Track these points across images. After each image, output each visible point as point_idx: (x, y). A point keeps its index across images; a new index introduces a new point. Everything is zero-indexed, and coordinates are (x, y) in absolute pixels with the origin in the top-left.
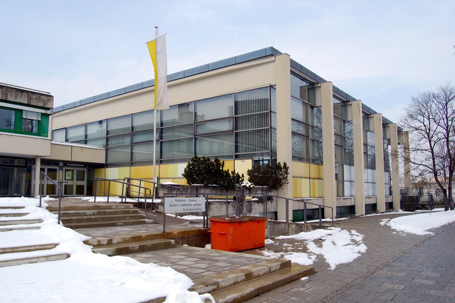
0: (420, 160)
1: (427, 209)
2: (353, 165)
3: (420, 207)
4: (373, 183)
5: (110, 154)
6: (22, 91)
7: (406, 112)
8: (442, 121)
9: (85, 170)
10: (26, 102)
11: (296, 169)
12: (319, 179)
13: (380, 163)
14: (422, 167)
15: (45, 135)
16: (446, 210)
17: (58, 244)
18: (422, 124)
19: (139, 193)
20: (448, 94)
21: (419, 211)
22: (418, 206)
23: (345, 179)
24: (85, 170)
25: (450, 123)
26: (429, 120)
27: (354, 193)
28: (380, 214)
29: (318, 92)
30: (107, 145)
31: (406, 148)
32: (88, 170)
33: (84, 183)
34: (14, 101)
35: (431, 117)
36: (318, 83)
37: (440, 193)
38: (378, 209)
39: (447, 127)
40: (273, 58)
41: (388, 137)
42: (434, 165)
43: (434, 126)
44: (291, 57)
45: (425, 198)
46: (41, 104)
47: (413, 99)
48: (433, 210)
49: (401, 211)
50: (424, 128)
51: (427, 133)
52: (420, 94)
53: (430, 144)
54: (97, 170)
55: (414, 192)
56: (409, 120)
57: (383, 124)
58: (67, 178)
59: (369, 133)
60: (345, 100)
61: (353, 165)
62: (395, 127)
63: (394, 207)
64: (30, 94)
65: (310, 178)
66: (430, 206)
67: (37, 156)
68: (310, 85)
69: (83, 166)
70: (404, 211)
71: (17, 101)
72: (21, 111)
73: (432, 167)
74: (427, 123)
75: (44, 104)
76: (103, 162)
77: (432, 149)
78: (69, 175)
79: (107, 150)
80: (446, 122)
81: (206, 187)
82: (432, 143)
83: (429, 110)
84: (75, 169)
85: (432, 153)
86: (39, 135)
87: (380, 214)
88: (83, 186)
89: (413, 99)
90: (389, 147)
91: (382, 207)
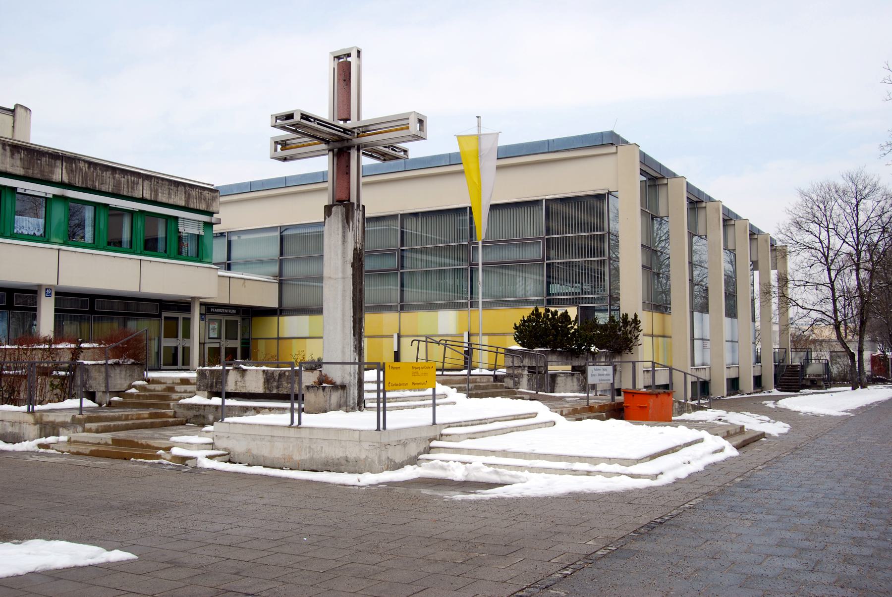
0: (811, 302)
1: (820, 387)
2: (707, 312)
3: (809, 383)
4: (732, 341)
5: (288, 291)
6: (177, 184)
7: (791, 217)
8: (850, 234)
9: (239, 319)
10: (182, 203)
11: (647, 321)
12: (664, 336)
13: (718, 300)
14: (815, 315)
15: (208, 260)
16: (853, 389)
17: (537, 414)
18: (818, 240)
19: (444, 363)
20: (860, 187)
21: (807, 391)
22: (804, 382)
23: (696, 337)
24: (239, 319)
25: (862, 236)
26: (828, 232)
27: (708, 360)
28: (746, 396)
29: (662, 192)
30: (281, 274)
31: (783, 280)
32: (243, 319)
33: (237, 344)
34: (130, 194)
35: (831, 226)
36: (663, 178)
37: (838, 360)
38: (741, 388)
39: (857, 245)
40: (613, 149)
41: (731, 247)
42: (835, 310)
43: (836, 243)
44: (640, 148)
45: (814, 369)
46: (203, 207)
47: (802, 193)
48: (829, 390)
49: (775, 392)
50: (818, 245)
51: (824, 254)
52: (813, 186)
53: (829, 274)
54: (255, 320)
55: (795, 359)
56: (794, 229)
57: (724, 220)
58: (212, 335)
59: (695, 239)
60: (695, 199)
61: (707, 312)
62: (766, 241)
63: (763, 384)
64: (188, 188)
65: (652, 336)
66: (824, 382)
67: (193, 298)
68: (654, 178)
69: (234, 311)
70: (781, 391)
71: (171, 202)
72: (176, 218)
73: (830, 314)
74: (824, 235)
75: (208, 206)
76: (275, 304)
77: (832, 282)
78: (214, 329)
79: (281, 284)
80: (855, 236)
81: (553, 352)
82: (833, 274)
83: (828, 214)
84: (224, 319)
85: (833, 289)
86: (201, 261)
87: (746, 396)
88: (236, 349)
89: (802, 193)
90: (756, 273)
91: (747, 384)
